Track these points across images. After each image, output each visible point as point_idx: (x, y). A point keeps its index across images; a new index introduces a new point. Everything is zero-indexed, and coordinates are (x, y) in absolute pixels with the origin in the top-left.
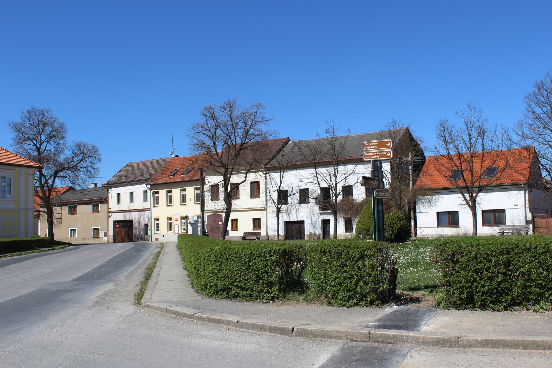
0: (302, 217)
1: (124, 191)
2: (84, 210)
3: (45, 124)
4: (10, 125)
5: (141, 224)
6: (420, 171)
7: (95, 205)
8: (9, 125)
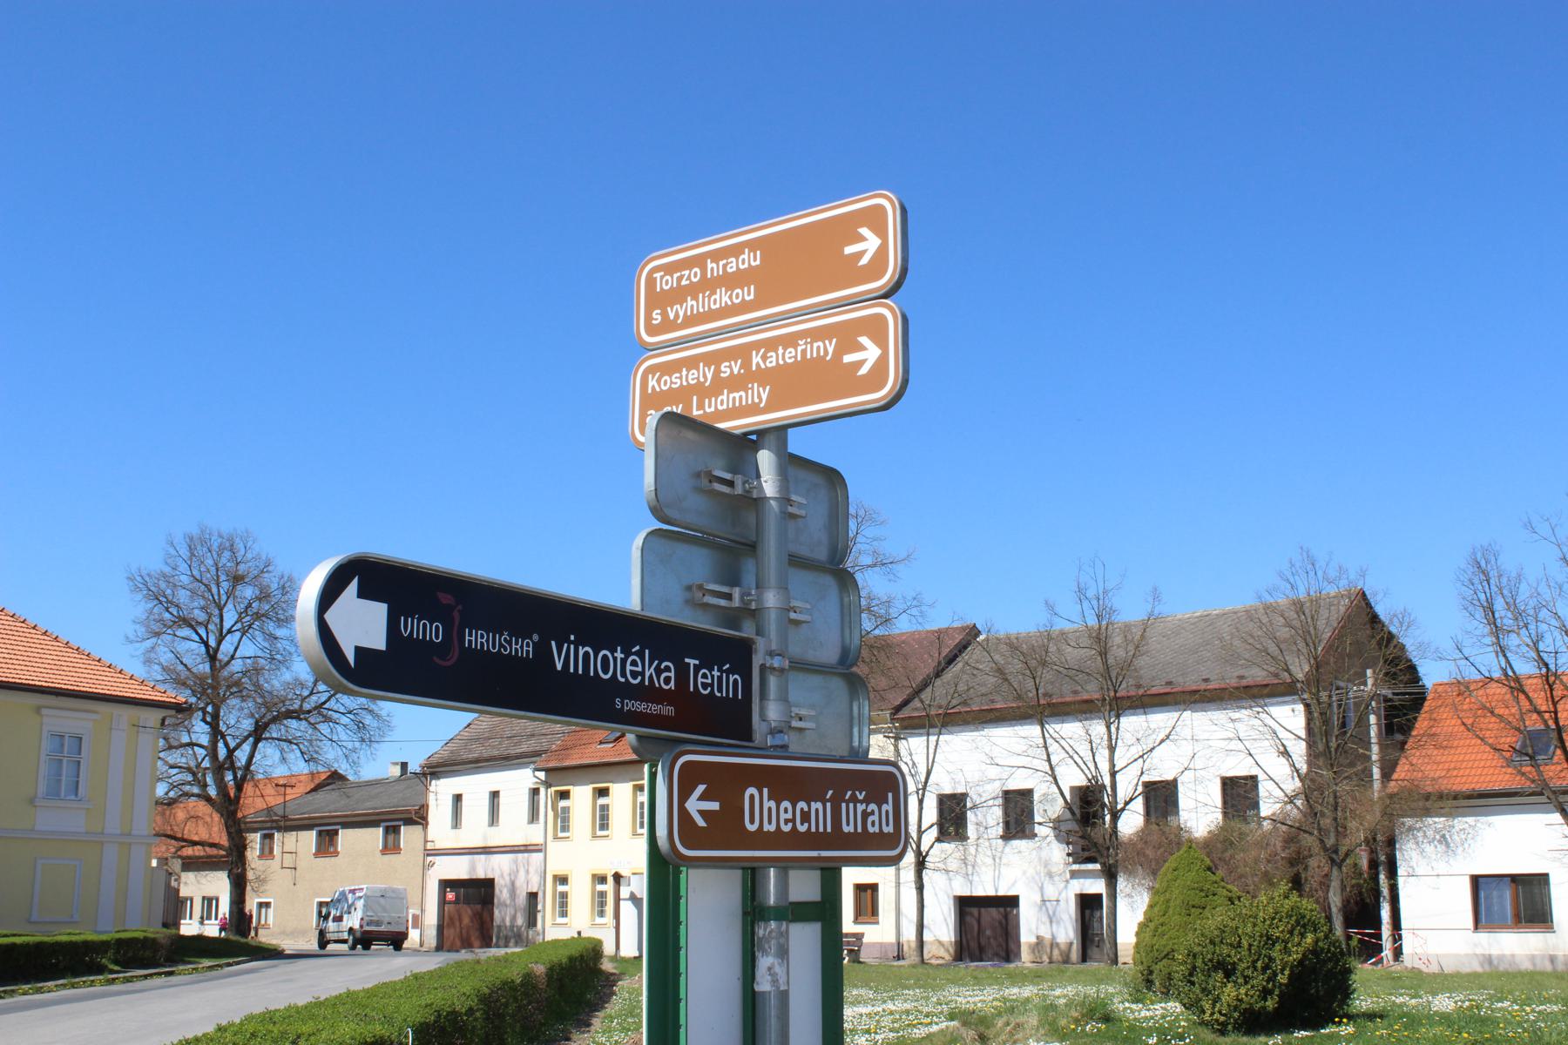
0: (1013, 885)
1: (475, 786)
2: (359, 843)
3: (237, 579)
4: (132, 581)
5: (518, 892)
6: (1406, 729)
7: (391, 829)
8: (128, 578)
